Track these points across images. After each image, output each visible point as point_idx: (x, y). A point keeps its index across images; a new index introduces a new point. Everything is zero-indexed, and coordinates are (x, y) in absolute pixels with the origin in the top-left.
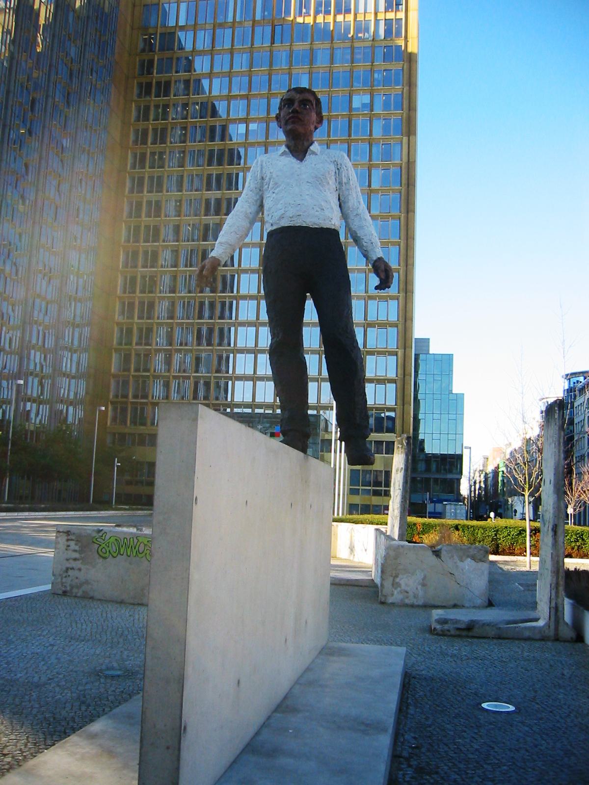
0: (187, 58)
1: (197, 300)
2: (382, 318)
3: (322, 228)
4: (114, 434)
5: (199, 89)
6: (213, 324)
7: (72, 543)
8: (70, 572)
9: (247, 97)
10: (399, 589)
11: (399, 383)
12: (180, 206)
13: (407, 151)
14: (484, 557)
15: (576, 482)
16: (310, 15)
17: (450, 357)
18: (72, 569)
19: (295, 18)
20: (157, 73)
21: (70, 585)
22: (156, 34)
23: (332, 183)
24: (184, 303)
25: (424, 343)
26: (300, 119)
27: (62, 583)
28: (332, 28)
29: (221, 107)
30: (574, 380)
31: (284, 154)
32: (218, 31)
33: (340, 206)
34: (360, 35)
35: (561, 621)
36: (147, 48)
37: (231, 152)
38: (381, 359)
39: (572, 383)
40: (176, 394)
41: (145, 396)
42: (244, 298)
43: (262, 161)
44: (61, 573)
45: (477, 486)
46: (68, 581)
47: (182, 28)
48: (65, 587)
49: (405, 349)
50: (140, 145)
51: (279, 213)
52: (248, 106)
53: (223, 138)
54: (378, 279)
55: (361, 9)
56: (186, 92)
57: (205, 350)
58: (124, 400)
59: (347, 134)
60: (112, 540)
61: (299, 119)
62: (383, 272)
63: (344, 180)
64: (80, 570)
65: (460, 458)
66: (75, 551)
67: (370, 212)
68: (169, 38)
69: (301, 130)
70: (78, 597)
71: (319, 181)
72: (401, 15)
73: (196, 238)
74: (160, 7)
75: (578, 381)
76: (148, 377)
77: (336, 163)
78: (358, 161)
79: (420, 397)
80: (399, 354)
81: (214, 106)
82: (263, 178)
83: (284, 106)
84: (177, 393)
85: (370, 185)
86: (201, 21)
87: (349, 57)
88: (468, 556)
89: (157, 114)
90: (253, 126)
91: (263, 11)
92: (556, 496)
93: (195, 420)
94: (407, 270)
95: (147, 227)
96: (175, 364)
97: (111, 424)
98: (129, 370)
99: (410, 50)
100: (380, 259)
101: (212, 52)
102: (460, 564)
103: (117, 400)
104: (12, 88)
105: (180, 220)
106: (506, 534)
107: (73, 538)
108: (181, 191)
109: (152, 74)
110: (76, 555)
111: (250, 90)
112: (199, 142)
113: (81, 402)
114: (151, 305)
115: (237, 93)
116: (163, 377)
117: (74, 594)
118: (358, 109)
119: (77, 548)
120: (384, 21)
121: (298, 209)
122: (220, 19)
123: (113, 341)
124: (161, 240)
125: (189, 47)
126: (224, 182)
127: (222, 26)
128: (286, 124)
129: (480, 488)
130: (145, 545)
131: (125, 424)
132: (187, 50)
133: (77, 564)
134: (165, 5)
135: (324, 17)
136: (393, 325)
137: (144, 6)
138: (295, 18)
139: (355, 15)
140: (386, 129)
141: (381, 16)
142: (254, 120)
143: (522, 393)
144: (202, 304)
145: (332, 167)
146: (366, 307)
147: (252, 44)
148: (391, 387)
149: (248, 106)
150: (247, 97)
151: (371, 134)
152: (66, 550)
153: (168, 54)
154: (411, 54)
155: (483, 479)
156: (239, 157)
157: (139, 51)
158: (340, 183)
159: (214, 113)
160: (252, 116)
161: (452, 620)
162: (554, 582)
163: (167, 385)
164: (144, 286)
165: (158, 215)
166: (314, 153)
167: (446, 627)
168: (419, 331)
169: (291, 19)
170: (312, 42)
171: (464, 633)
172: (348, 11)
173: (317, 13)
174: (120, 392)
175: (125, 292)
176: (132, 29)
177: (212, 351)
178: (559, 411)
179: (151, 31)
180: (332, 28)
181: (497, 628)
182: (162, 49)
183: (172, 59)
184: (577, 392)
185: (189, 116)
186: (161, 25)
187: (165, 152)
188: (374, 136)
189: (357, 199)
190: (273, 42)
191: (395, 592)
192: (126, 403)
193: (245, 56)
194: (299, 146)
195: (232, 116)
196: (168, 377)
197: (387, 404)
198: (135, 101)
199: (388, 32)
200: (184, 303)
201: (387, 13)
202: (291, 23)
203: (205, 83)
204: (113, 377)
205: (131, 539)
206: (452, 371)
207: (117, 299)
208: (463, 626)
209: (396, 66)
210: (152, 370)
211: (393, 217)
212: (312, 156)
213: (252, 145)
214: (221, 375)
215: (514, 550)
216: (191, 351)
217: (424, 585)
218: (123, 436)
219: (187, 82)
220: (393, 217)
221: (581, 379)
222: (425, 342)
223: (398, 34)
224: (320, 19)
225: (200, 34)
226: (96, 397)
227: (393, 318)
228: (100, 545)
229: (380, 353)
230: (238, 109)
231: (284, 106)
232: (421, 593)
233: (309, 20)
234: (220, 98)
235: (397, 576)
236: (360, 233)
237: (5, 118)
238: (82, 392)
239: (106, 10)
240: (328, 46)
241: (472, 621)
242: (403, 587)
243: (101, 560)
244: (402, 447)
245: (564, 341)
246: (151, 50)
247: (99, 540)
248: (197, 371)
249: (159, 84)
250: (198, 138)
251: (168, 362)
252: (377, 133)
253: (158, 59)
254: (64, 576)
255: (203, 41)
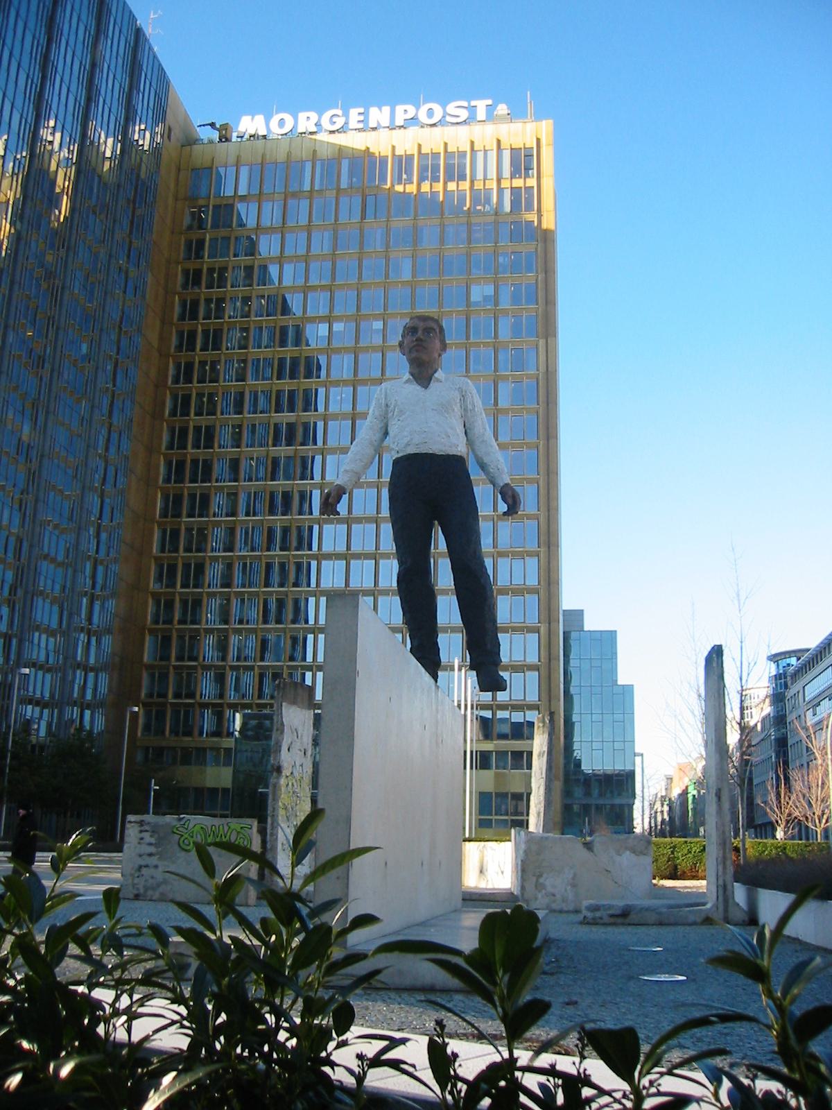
0: (249, 238)
1: (264, 561)
2: (518, 580)
3: (448, 456)
4: (147, 749)
5: (265, 279)
6: (286, 594)
7: (147, 836)
8: (144, 871)
9: (330, 289)
10: (544, 891)
11: (544, 671)
12: (240, 433)
13: (545, 358)
14: (646, 848)
15: (785, 794)
16: (413, 183)
17: (612, 635)
18: (147, 866)
19: (393, 186)
20: (208, 258)
21: (144, 887)
22: (207, 206)
23: (457, 408)
24: (245, 565)
25: (576, 616)
26: (424, 348)
27: (134, 885)
28: (441, 199)
29: (295, 302)
30: (783, 663)
31: (408, 381)
32: (291, 203)
33: (466, 433)
34: (479, 208)
35: (731, 901)
36: (195, 224)
37: (308, 360)
38: (518, 638)
39: (781, 667)
40: (233, 693)
41: (191, 695)
42: (329, 556)
43: (386, 389)
44: (133, 872)
45: (659, 819)
46: (141, 883)
47: (243, 198)
48: (138, 889)
49: (549, 624)
50: (186, 351)
51: (405, 440)
52: (332, 299)
53: (297, 342)
54: (506, 506)
55: (480, 175)
56: (247, 282)
57: (276, 630)
58: (161, 700)
59: (465, 338)
60: (197, 828)
61: (422, 347)
62: (511, 499)
63: (470, 407)
64: (156, 867)
65: (631, 775)
66: (150, 844)
67: (497, 440)
68: (225, 211)
69: (424, 357)
70: (155, 901)
71: (445, 408)
72: (532, 182)
73: (261, 475)
74: (214, 172)
75: (789, 665)
76: (195, 667)
77: (461, 390)
78: (480, 372)
79: (572, 690)
80: (542, 630)
81: (284, 300)
82: (387, 405)
83: (408, 334)
84: (235, 690)
85: (496, 403)
86: (267, 189)
87: (465, 235)
88: (627, 848)
89: (208, 312)
90: (338, 327)
91: (351, 175)
92: (718, 755)
93: (357, 606)
94: (549, 516)
95: (195, 462)
96: (232, 652)
97: (142, 734)
98: (168, 658)
99: (544, 226)
100: (507, 485)
101: (282, 229)
102: (617, 858)
103: (151, 700)
104: (17, 278)
105: (241, 451)
106: (686, 852)
107: (147, 828)
108: (240, 413)
109: (202, 257)
110: (152, 849)
111: (334, 279)
112: (265, 347)
113: (101, 704)
114: (200, 569)
115: (317, 283)
116: (216, 667)
117: (148, 898)
118: (477, 304)
119: (153, 840)
120: (509, 190)
121: (424, 436)
122: (294, 187)
123: (146, 617)
124: (214, 480)
125: (251, 223)
126: (300, 403)
127: (295, 195)
128: (410, 352)
129: (663, 821)
130: (238, 833)
131: (163, 733)
132: (249, 226)
133: (154, 860)
134: (219, 169)
135: (431, 184)
136: (532, 591)
137: (192, 170)
138: (393, 186)
139: (472, 182)
140: (516, 329)
141: (505, 184)
142: (339, 319)
143: (696, 663)
144: (269, 567)
145: (457, 395)
146: (495, 534)
147: (336, 220)
148: (533, 676)
149: (332, 299)
150: (330, 289)
151: (496, 336)
152: (139, 843)
153: (223, 232)
154: (546, 232)
155: (666, 808)
156: (319, 368)
157: (184, 228)
158: (465, 410)
159: (285, 310)
160: (336, 313)
161: (604, 905)
162: (721, 855)
163: (220, 679)
164: (190, 542)
165: (209, 445)
166: (438, 380)
167: (598, 914)
168: (569, 600)
169: (388, 187)
170: (416, 215)
171: (620, 920)
172: (462, 177)
173: (421, 179)
174: (156, 689)
175: (163, 551)
176: (176, 199)
177: (284, 630)
178: (718, 658)
179: (201, 202)
180: (441, 199)
181: (657, 913)
182: (215, 225)
183: (229, 238)
184: (789, 678)
185: (253, 313)
186: (215, 193)
187: (219, 361)
188: (501, 339)
189: (483, 426)
190: (363, 217)
191: (540, 896)
192: (164, 705)
193: (326, 234)
194: (423, 372)
195: (310, 313)
196: (224, 668)
197: (527, 699)
198: (179, 294)
199: (515, 203)
200: (245, 565)
201: (513, 180)
202: (387, 192)
203: (273, 270)
204: (146, 669)
205: (221, 827)
206: (616, 653)
207: (153, 560)
208: (618, 912)
209: (527, 248)
210: (201, 659)
211: (529, 446)
212: (436, 384)
213: (338, 351)
214: (297, 664)
215: (698, 871)
216: (254, 631)
217: (574, 886)
218: (160, 752)
219: (249, 270)
220: (529, 446)
221: (793, 661)
222: (578, 615)
223: (529, 208)
224: (426, 187)
225: (267, 207)
226: (124, 693)
227: (532, 581)
228: (182, 836)
229: (515, 629)
230: (318, 304)
231: (408, 334)
232: (571, 896)
233: (411, 188)
234: (294, 289)
235: (540, 876)
236: (486, 460)
237: (7, 316)
238: (103, 688)
239: (143, 176)
240: (437, 222)
241: (627, 905)
242: (550, 889)
243: (183, 853)
244: (543, 726)
245: (738, 592)
246: (200, 228)
247: (180, 829)
248: (262, 659)
249: (211, 271)
250: (265, 341)
251: (223, 647)
252: (505, 333)
253: (210, 239)
254: (136, 875)
255: (271, 214)
